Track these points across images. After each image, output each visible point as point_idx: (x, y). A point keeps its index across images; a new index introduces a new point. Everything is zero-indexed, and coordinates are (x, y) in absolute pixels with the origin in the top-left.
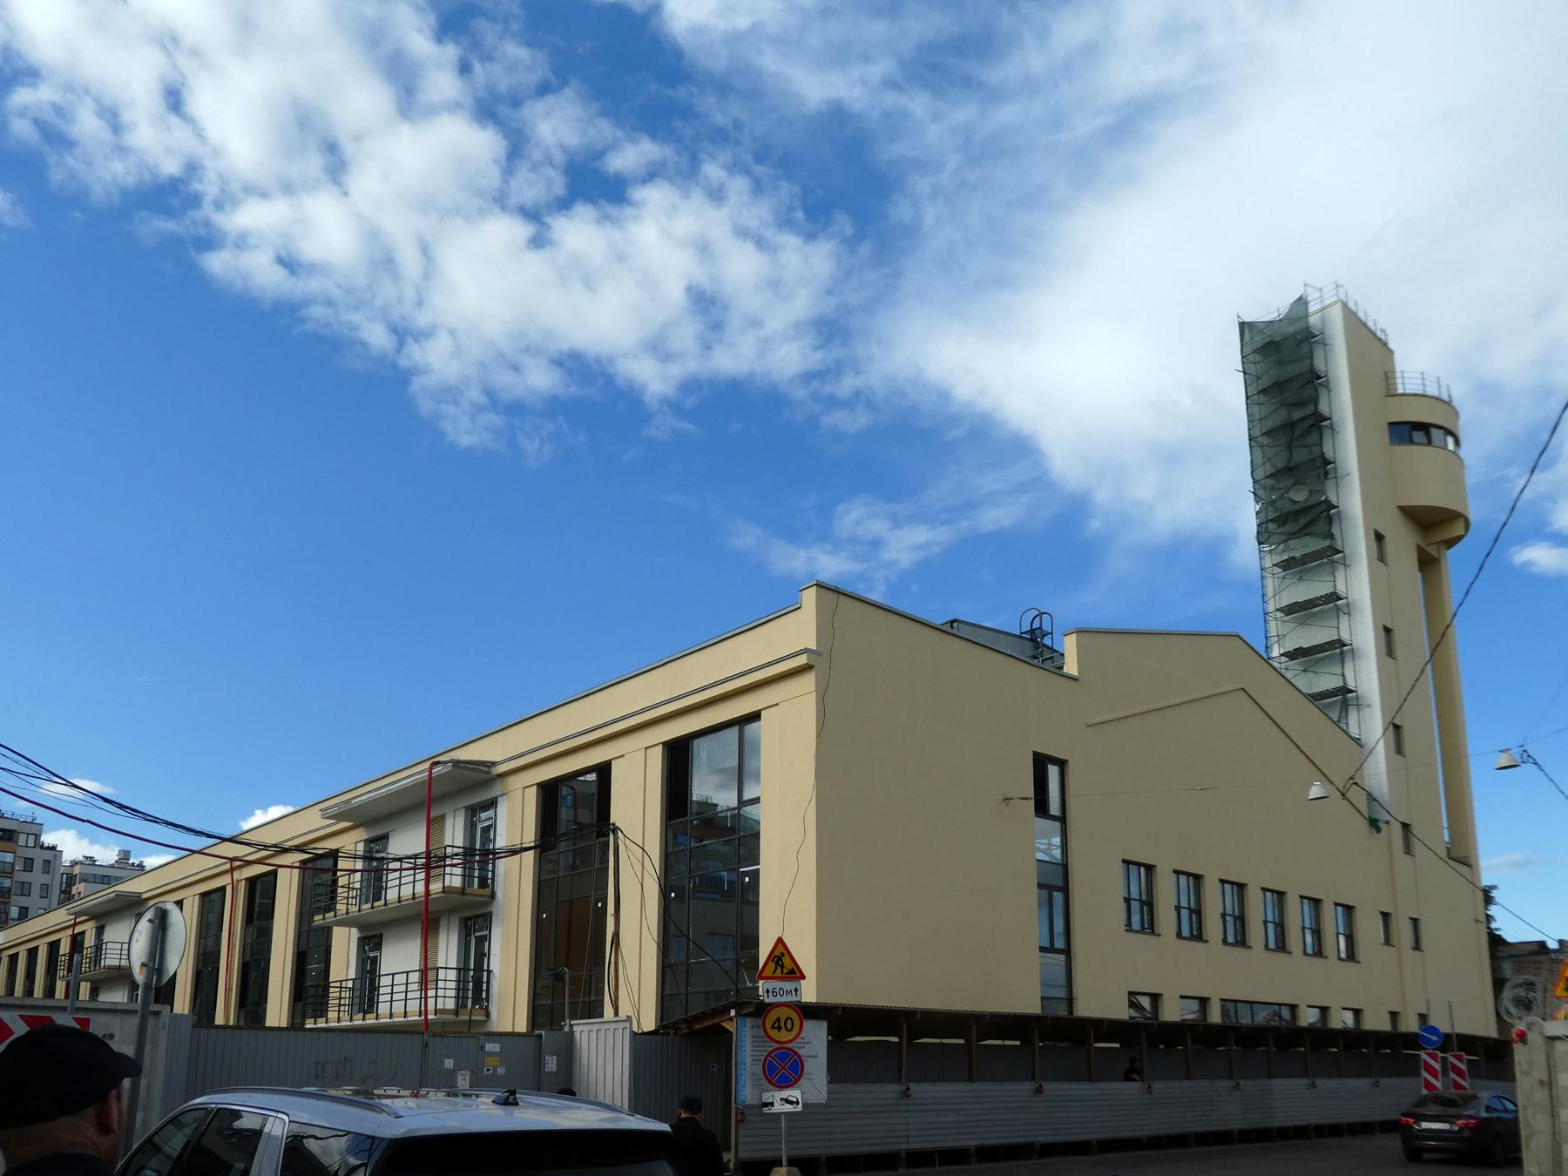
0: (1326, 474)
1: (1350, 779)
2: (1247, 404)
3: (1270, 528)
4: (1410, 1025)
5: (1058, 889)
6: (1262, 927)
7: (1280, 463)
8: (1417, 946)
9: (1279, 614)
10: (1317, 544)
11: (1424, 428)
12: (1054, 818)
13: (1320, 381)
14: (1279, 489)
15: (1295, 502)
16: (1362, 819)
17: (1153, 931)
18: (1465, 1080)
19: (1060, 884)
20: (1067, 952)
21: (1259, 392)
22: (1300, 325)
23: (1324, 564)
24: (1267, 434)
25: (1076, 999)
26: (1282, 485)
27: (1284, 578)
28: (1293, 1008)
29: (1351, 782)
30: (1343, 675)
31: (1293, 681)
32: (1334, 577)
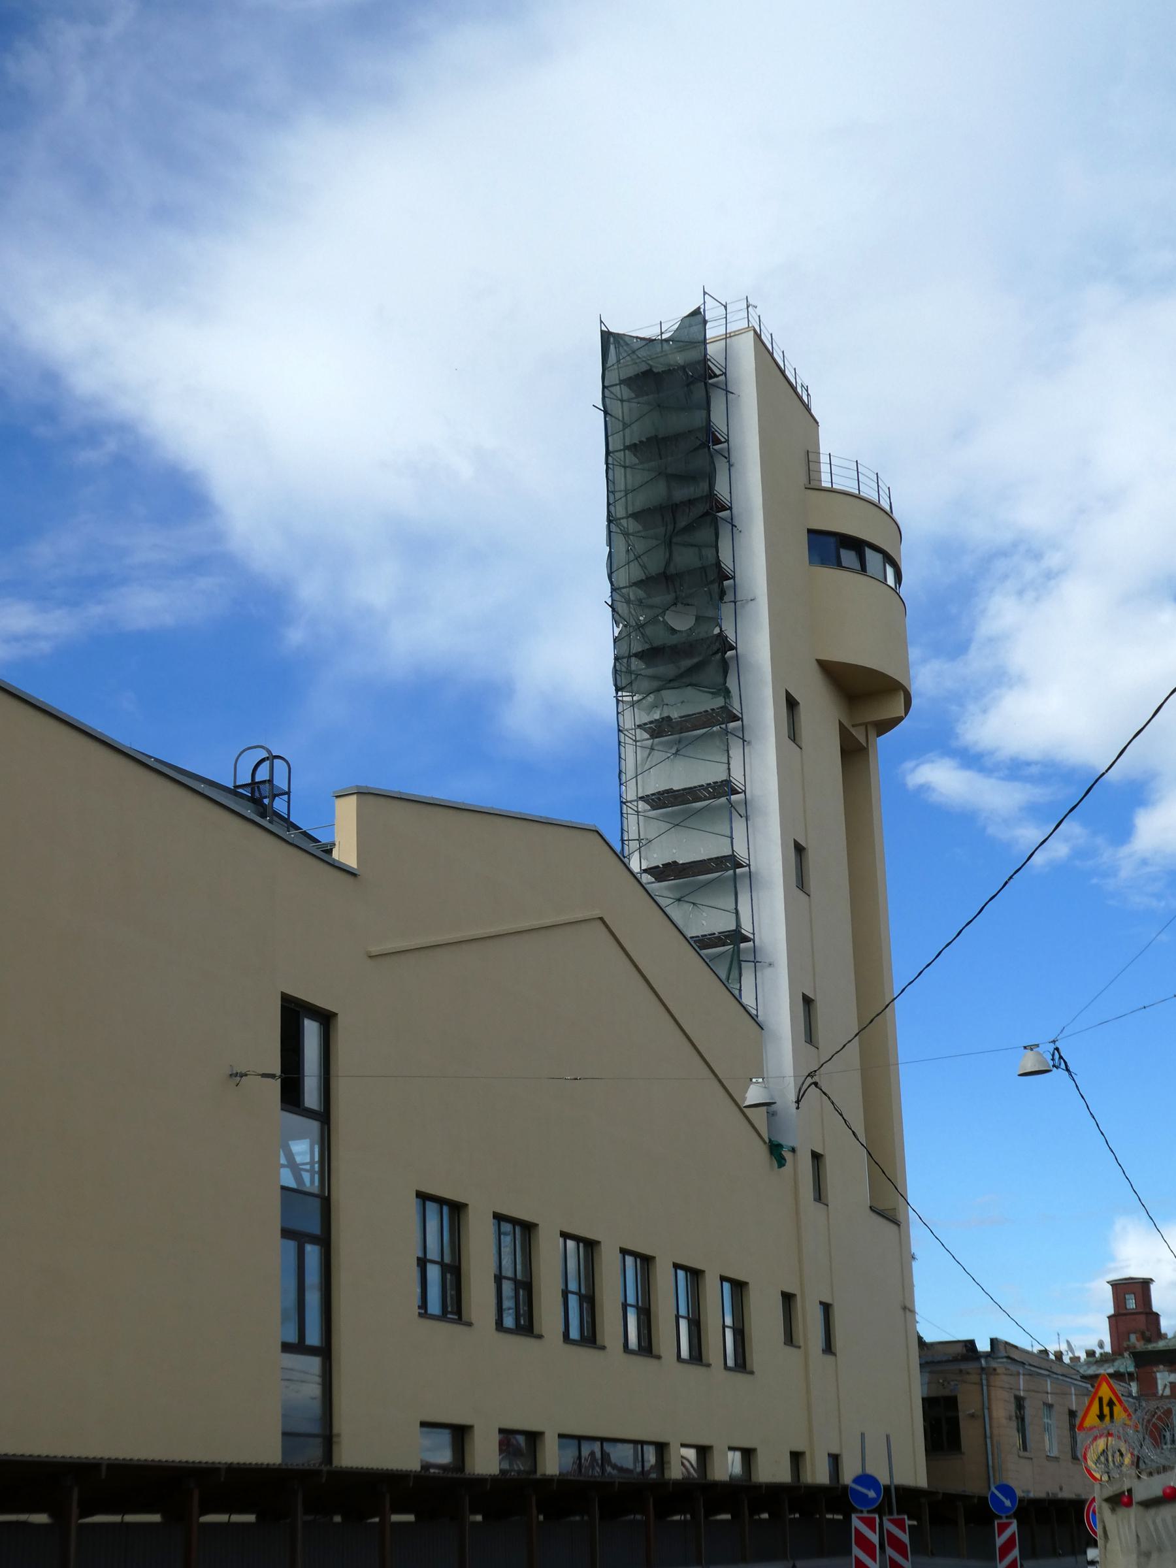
0: (722, 593)
1: (809, 1075)
2: (607, 463)
3: (633, 667)
4: (818, 1474)
5: (313, 1239)
6: (560, 1299)
7: (655, 564)
8: (829, 1348)
9: (642, 806)
10: (709, 703)
11: (857, 545)
12: (309, 1113)
13: (716, 447)
14: (651, 607)
15: (673, 631)
16: (761, 1143)
17: (460, 1318)
18: (906, 1558)
19: (315, 1228)
20: (325, 1352)
21: (626, 448)
22: (693, 355)
23: (713, 734)
24: (635, 516)
25: (339, 1435)
26: (657, 600)
27: (652, 749)
28: (661, 1448)
29: (809, 1080)
30: (737, 913)
31: (668, 910)
32: (728, 756)
